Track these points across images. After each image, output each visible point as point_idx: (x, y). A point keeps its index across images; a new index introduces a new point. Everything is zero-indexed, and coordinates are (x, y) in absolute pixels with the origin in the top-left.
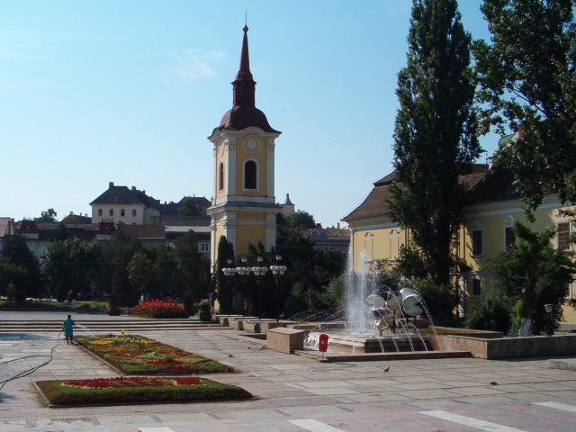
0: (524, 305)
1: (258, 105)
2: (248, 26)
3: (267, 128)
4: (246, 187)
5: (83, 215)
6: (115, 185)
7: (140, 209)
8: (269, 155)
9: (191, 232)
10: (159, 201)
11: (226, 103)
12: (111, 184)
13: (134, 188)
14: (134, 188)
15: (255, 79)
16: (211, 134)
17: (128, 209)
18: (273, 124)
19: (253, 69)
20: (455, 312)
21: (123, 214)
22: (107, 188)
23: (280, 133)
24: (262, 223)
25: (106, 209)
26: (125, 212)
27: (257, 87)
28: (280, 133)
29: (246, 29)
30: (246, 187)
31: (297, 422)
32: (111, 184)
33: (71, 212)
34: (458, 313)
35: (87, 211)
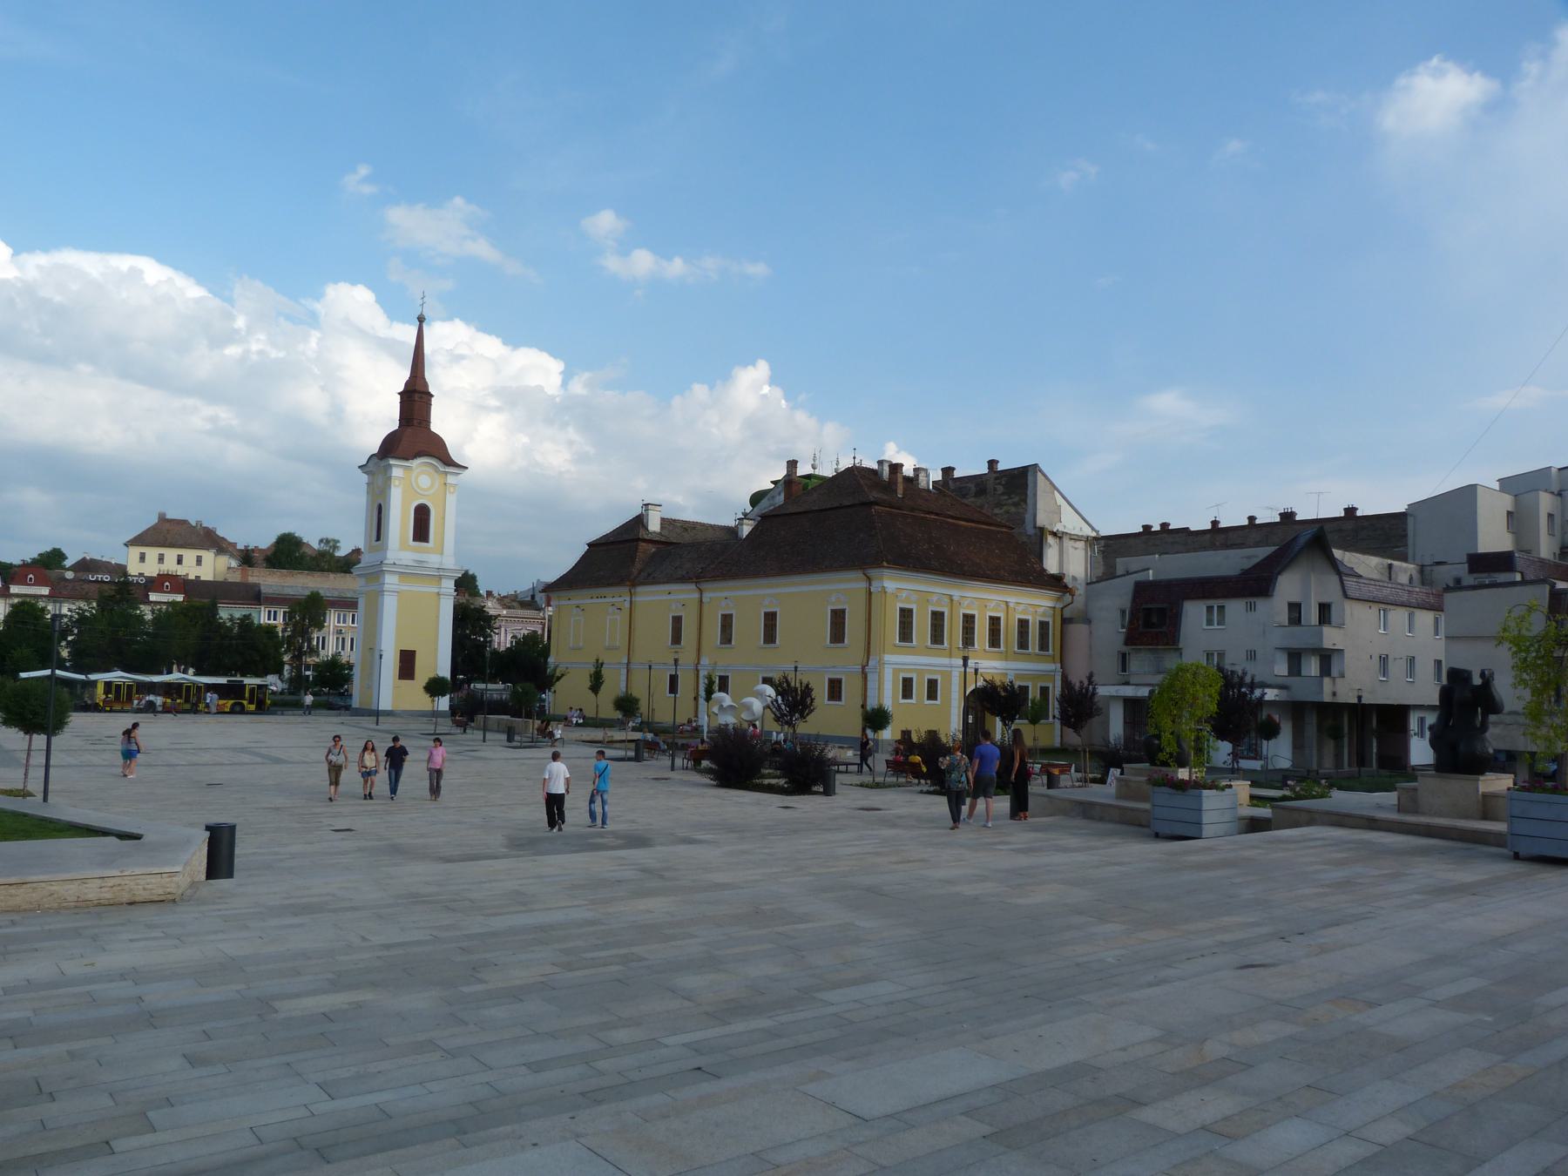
7: (208, 556)
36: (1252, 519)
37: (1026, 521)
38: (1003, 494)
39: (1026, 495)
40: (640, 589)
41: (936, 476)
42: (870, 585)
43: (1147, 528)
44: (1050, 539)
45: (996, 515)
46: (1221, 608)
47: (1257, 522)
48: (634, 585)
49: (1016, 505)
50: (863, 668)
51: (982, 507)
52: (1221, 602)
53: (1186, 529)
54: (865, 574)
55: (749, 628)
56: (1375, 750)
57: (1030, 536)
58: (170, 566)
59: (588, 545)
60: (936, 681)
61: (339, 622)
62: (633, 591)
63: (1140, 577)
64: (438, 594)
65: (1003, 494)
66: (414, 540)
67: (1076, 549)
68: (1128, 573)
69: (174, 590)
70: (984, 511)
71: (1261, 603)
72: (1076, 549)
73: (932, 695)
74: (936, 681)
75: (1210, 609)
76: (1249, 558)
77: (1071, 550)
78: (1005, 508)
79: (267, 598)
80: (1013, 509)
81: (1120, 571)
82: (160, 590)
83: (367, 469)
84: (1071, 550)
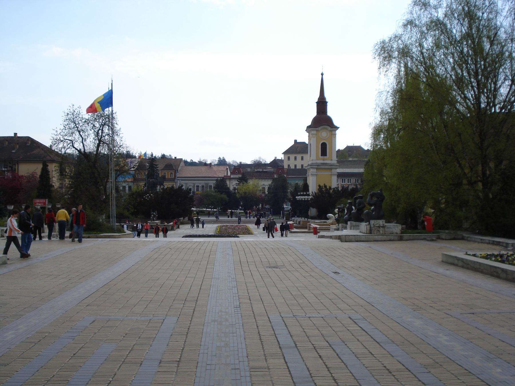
1: (329, 114)
2: (324, 73)
4: (321, 156)
6: (298, 141)
8: (333, 138)
11: (314, 113)
12: (295, 141)
14: (175, 158)
15: (327, 100)
16: (306, 129)
18: (336, 123)
19: (326, 95)
22: (293, 143)
24: (330, 173)
25: (292, 157)
27: (328, 104)
28: (339, 128)
29: (322, 74)
30: (321, 156)
31: (37, 231)
32: (295, 141)
33: (276, 157)
35: (281, 157)
61: (343, 182)
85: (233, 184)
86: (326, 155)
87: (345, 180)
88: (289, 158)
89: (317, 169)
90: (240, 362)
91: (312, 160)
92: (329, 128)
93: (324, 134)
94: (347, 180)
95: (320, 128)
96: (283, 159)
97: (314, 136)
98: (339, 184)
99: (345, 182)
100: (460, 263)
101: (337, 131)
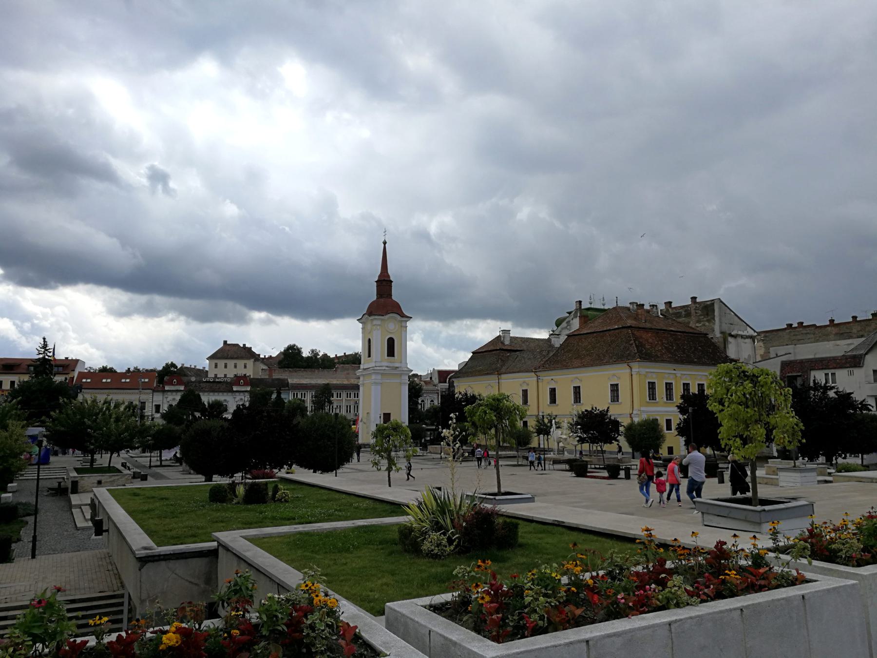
0: (845, 451)
3: (403, 315)
5: (193, 367)
6: (247, 346)
7: (250, 363)
9: (665, 491)
10: (259, 355)
12: (225, 342)
13: (244, 345)
14: (244, 345)
17: (241, 363)
20: (233, 402)
21: (245, 367)
23: (411, 318)
25: (221, 363)
26: (247, 366)
29: (385, 243)
32: (225, 342)
34: (55, 412)
36: (854, 318)
37: (715, 329)
38: (701, 315)
39: (714, 316)
40: (503, 376)
41: (662, 307)
42: (631, 371)
43: (790, 326)
44: (730, 339)
45: (697, 327)
46: (833, 374)
47: (858, 319)
48: (500, 374)
49: (708, 321)
50: (631, 415)
51: (689, 323)
52: (833, 371)
53: (814, 325)
54: (628, 365)
55: (565, 396)
56: (692, 436)
57: (718, 338)
58: (241, 371)
59: (473, 353)
60: (670, 420)
61: (347, 397)
62: (499, 377)
63: (784, 358)
64: (401, 383)
65: (701, 315)
66: (388, 356)
67: (746, 343)
68: (777, 356)
69: (245, 384)
70: (690, 325)
71: (856, 371)
72: (746, 343)
73: (652, 386)
74: (670, 420)
75: (826, 375)
76: (849, 345)
77: (743, 344)
78: (702, 323)
79: (293, 386)
80: (707, 324)
81: (772, 355)
82: (238, 384)
83: (362, 321)
84: (743, 344)
85: (168, 399)
86: (11, 381)
87: (350, 394)
88: (216, 366)
89: (382, 374)
90: (585, 644)
91: (376, 362)
92: (399, 317)
93: (388, 325)
94: (352, 395)
95: (386, 317)
96: (207, 369)
97: (378, 327)
98: (343, 399)
99: (350, 397)
100: (870, 480)
101: (408, 324)
